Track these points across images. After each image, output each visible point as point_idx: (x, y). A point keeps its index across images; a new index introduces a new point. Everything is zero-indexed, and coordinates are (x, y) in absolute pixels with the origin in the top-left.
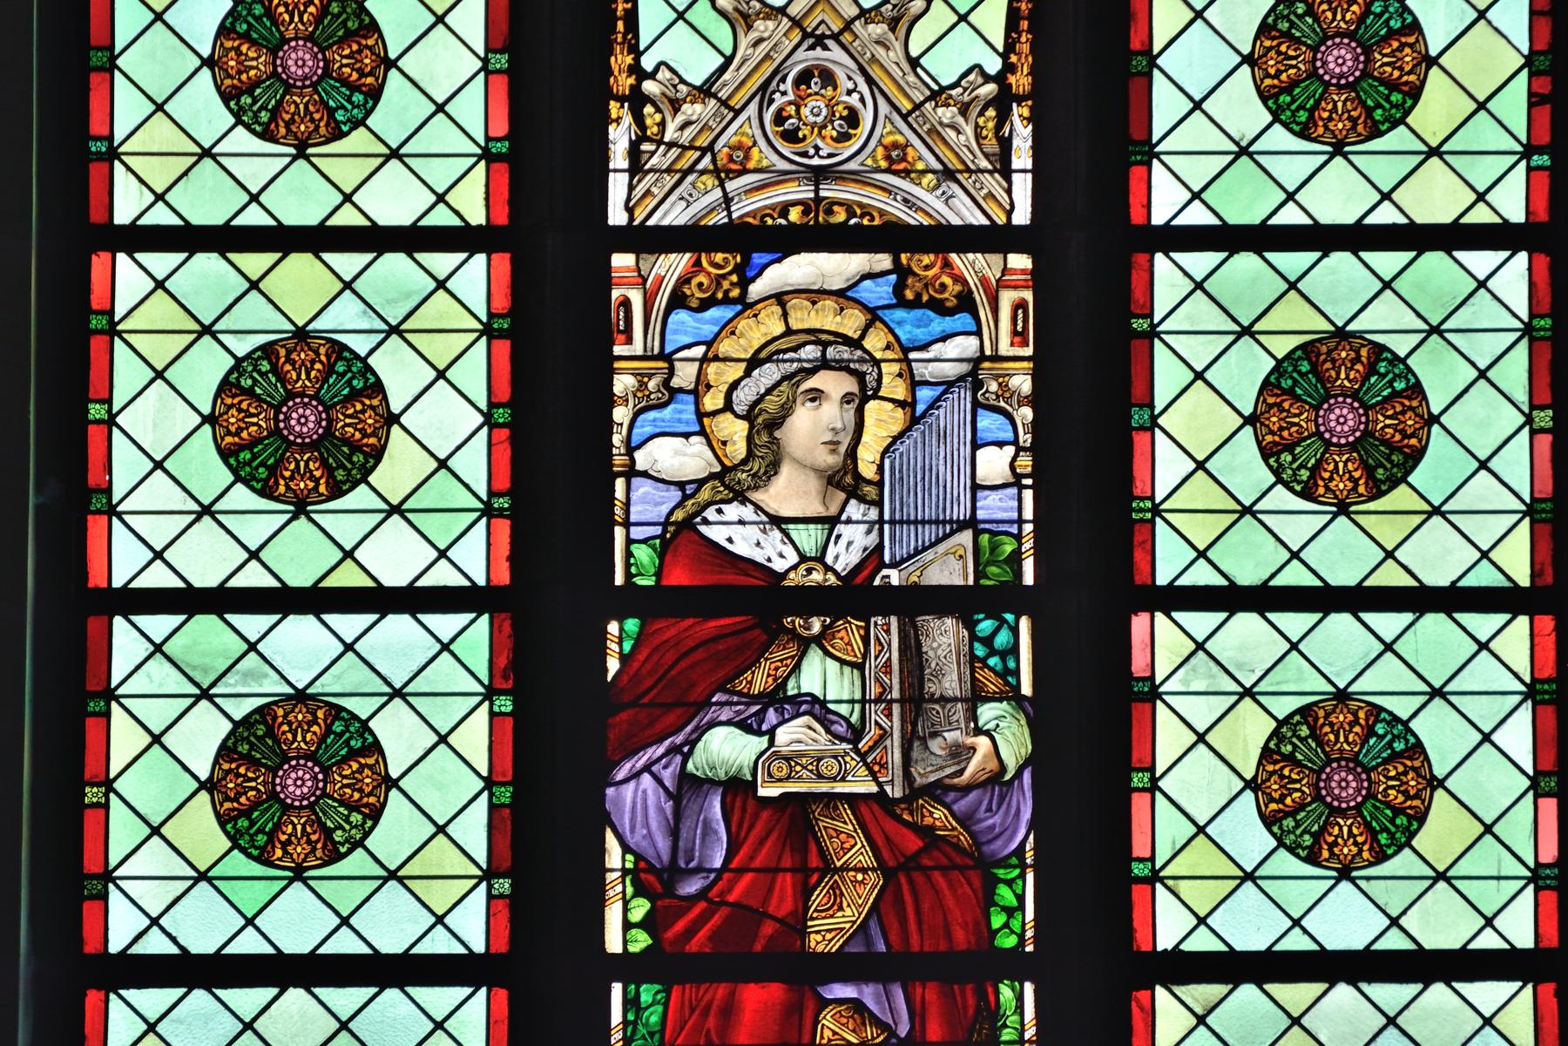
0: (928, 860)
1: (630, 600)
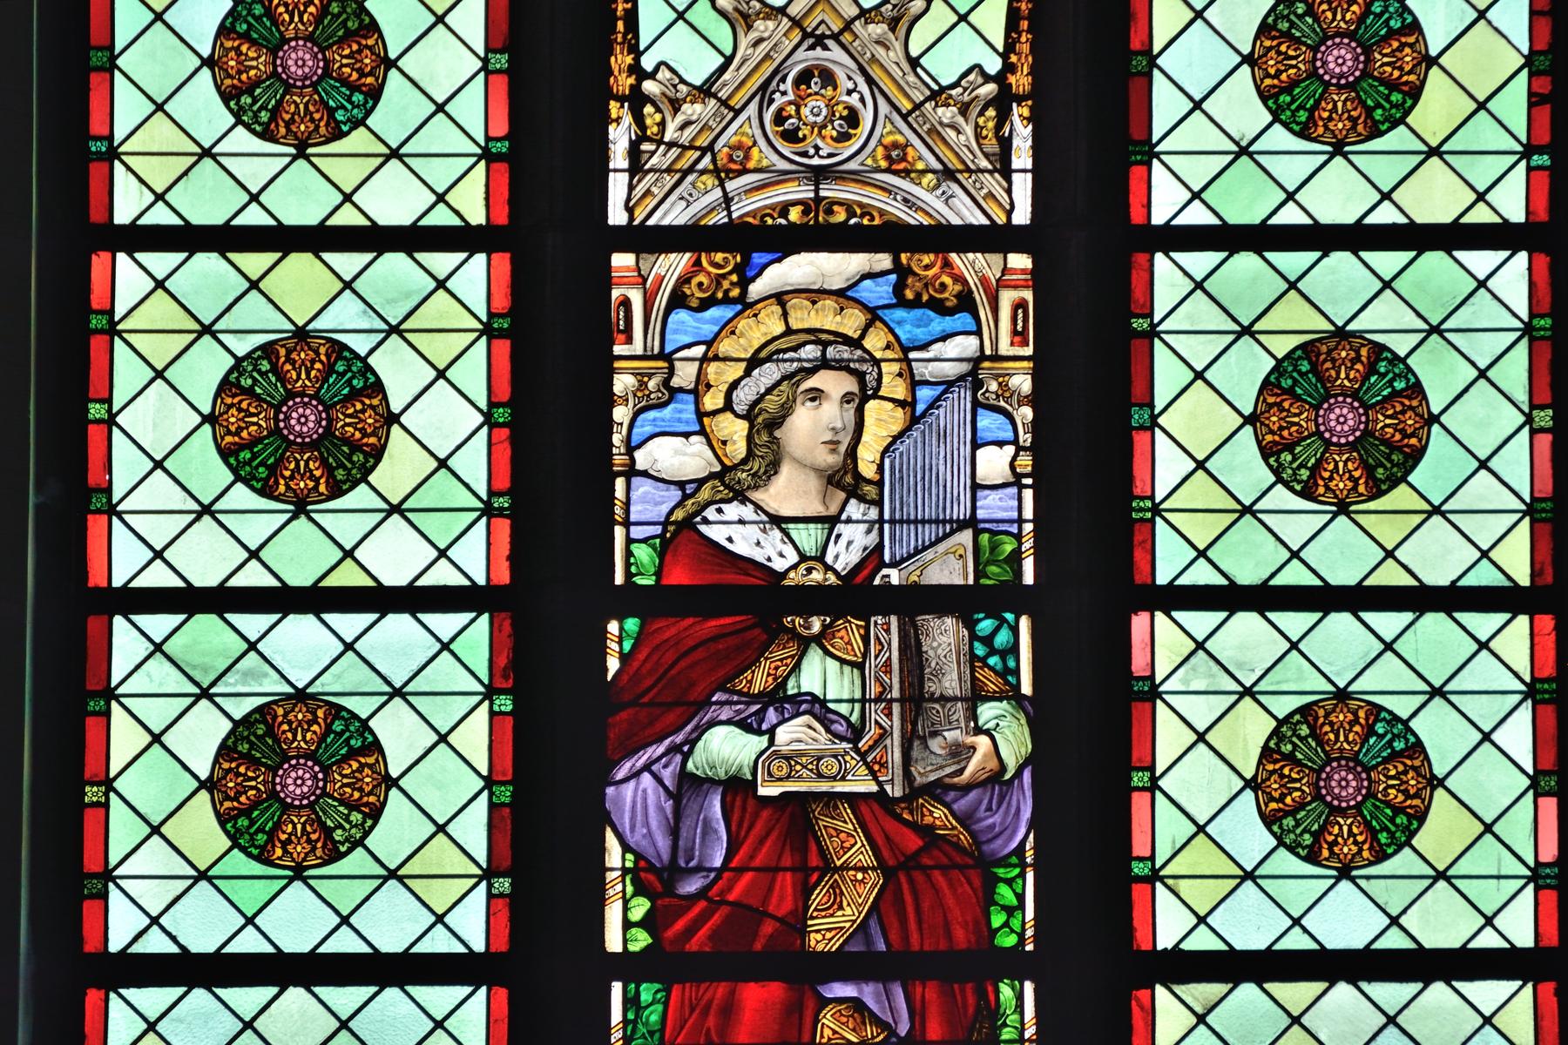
0: (928, 860)
1: (630, 600)
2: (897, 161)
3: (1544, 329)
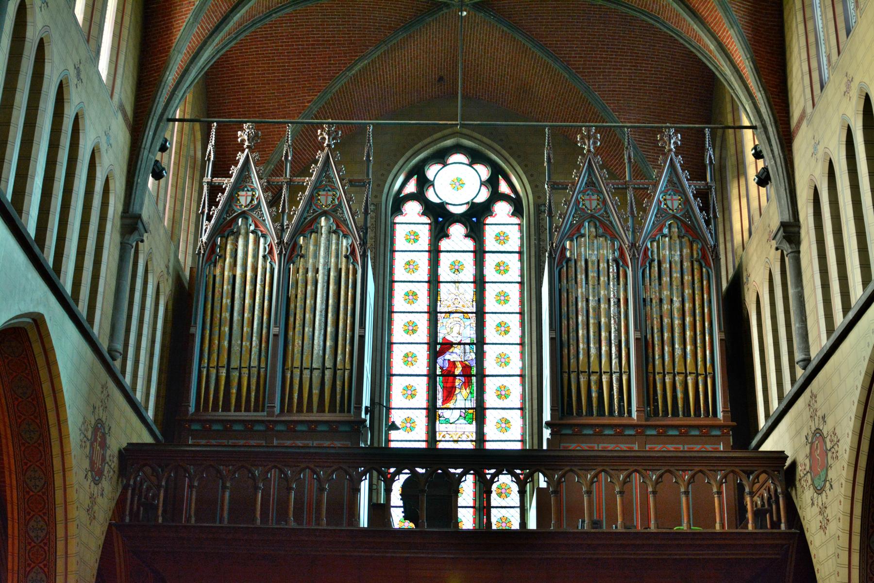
0: (466, 368)
1: (439, 344)
2: (463, 306)
3: (483, 508)
